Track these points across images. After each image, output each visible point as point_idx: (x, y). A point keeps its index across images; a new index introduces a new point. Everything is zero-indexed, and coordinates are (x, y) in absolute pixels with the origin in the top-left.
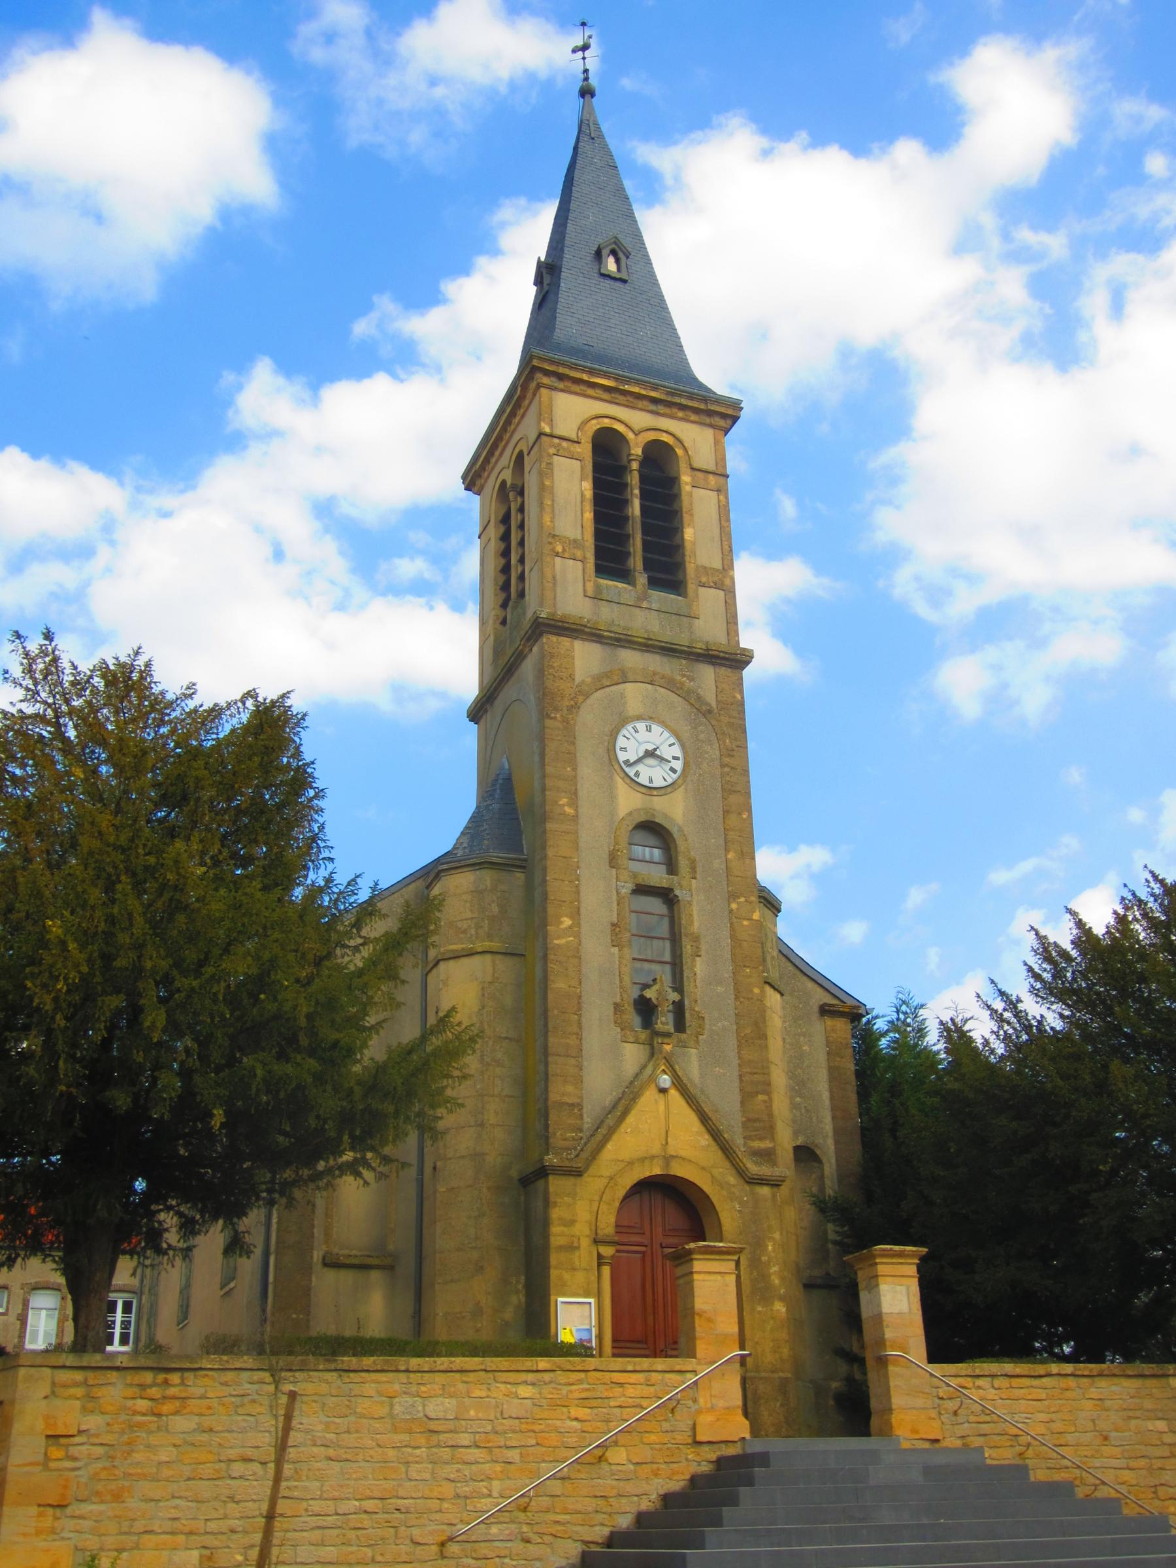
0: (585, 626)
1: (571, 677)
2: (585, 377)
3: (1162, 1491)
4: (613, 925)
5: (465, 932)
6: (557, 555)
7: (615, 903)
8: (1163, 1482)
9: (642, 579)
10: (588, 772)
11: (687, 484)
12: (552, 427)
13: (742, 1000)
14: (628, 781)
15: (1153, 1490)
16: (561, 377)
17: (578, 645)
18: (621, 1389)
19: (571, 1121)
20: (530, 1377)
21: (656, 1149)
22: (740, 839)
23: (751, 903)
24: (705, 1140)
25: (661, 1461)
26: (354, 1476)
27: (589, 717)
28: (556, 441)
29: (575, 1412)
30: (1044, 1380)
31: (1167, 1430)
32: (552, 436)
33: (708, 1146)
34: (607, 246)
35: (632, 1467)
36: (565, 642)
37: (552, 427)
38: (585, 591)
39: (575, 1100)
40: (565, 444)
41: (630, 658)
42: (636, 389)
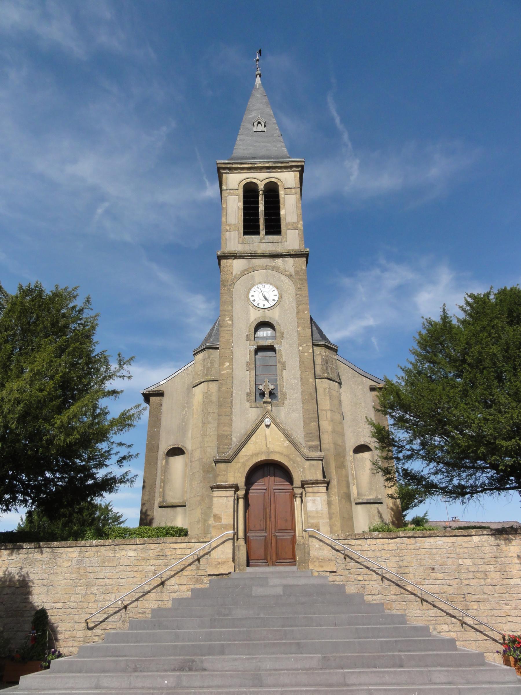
0: (237, 254)
1: (232, 273)
2: (239, 166)
3: (468, 597)
4: (247, 363)
5: (200, 375)
6: (227, 231)
7: (248, 354)
8: (469, 592)
9: (262, 232)
10: (238, 306)
11: (282, 194)
12: (227, 187)
13: (304, 385)
14: (255, 307)
15: (463, 596)
16: (230, 169)
17: (235, 261)
18: (175, 551)
19: (226, 441)
20: (134, 547)
21: (264, 449)
22: (303, 322)
23: (308, 346)
24: (287, 443)
25: (191, 583)
26: (53, 593)
27: (239, 287)
28: (228, 191)
29: (153, 562)
30: (396, 540)
31: (471, 564)
32: (226, 190)
33: (288, 445)
34: (256, 122)
35: (177, 586)
36: (230, 261)
37: (227, 187)
38: (239, 241)
39: (229, 433)
40: (232, 191)
41: (257, 262)
42: (259, 165)
